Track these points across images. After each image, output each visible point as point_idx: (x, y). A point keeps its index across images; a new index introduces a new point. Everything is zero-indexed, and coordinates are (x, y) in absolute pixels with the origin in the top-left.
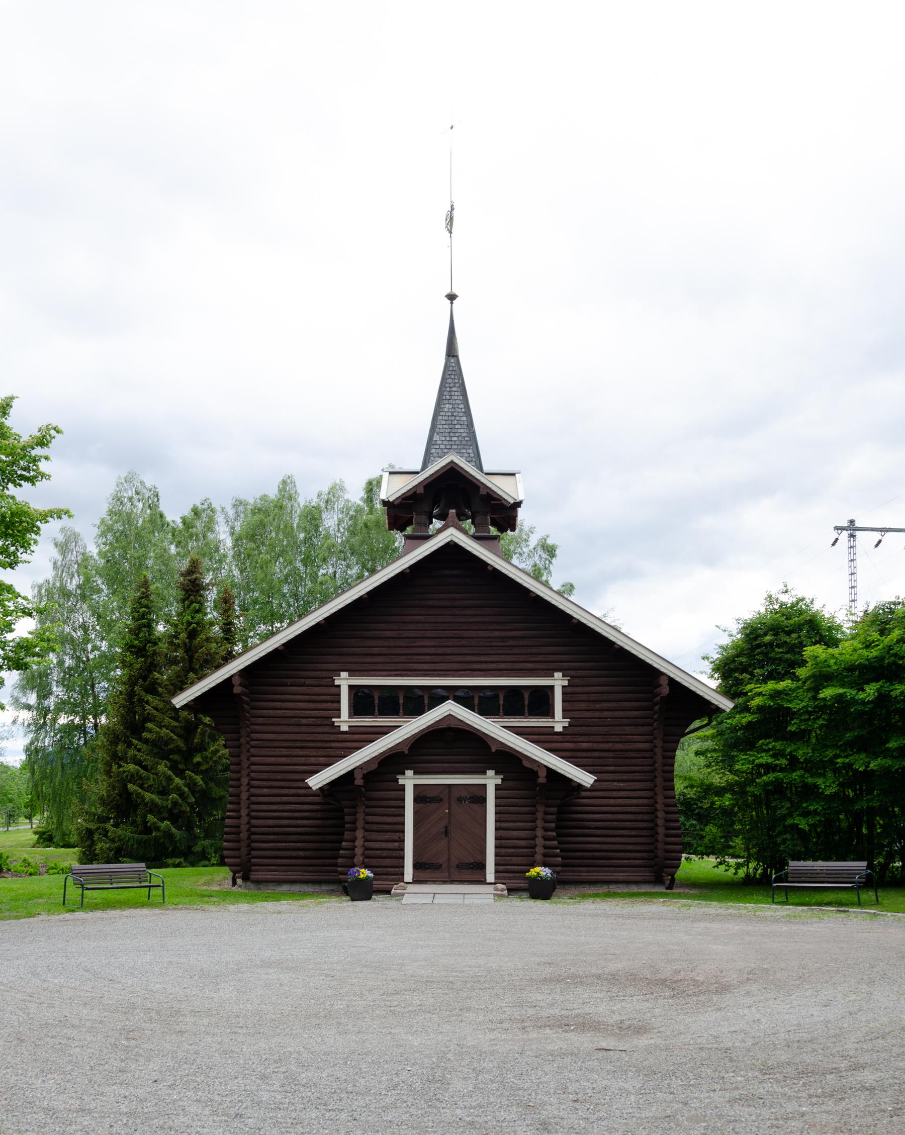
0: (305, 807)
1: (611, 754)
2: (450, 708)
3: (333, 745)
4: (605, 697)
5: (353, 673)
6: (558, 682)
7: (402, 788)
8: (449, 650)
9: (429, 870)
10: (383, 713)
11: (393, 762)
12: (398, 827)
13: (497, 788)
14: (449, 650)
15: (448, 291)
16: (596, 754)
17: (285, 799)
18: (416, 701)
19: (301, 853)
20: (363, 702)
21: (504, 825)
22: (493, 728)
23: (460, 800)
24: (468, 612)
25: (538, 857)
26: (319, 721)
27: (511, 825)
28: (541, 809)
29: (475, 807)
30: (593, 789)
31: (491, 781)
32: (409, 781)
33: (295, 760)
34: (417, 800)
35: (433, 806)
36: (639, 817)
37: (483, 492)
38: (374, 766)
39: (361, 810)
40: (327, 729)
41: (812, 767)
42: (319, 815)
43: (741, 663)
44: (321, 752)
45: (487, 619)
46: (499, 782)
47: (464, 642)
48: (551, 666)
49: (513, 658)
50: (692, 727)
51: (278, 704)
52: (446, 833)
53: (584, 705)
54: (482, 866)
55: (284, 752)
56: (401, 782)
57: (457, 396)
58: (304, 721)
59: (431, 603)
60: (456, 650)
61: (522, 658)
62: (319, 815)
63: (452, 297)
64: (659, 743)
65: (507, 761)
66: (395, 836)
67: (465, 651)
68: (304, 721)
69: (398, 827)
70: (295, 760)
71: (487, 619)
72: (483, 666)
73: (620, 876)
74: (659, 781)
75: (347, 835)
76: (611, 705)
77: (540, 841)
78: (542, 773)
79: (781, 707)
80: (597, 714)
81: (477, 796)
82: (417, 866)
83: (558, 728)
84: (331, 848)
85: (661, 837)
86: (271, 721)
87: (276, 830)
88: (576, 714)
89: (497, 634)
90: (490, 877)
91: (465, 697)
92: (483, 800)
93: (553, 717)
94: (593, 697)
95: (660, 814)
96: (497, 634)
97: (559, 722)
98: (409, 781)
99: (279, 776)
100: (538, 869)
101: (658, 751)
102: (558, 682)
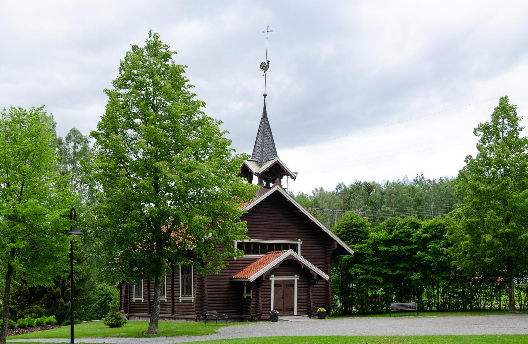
0: (223, 290)
2: (289, 252)
4: (312, 248)
6: (299, 242)
8: (267, 230)
9: (301, 313)
10: (255, 253)
11: (274, 271)
12: (269, 296)
13: (298, 281)
14: (267, 230)
15: (264, 93)
17: (216, 286)
19: (222, 308)
23: (287, 285)
24: (273, 215)
29: (291, 288)
31: (296, 278)
32: (273, 278)
34: (275, 285)
35: (279, 288)
36: (322, 291)
39: (260, 290)
41: (375, 274)
45: (278, 218)
47: (272, 227)
48: (297, 236)
49: (286, 233)
52: (283, 298)
54: (293, 309)
56: (270, 279)
59: (262, 211)
61: (289, 233)
63: (265, 96)
67: (272, 230)
69: (269, 296)
71: (278, 218)
72: (278, 236)
78: (316, 276)
79: (362, 252)
80: (310, 254)
81: (291, 284)
84: (241, 303)
87: (213, 299)
89: (281, 224)
90: (296, 313)
92: (293, 285)
94: (309, 248)
96: (281, 224)
98: (273, 278)
101: (329, 268)
102: (299, 242)
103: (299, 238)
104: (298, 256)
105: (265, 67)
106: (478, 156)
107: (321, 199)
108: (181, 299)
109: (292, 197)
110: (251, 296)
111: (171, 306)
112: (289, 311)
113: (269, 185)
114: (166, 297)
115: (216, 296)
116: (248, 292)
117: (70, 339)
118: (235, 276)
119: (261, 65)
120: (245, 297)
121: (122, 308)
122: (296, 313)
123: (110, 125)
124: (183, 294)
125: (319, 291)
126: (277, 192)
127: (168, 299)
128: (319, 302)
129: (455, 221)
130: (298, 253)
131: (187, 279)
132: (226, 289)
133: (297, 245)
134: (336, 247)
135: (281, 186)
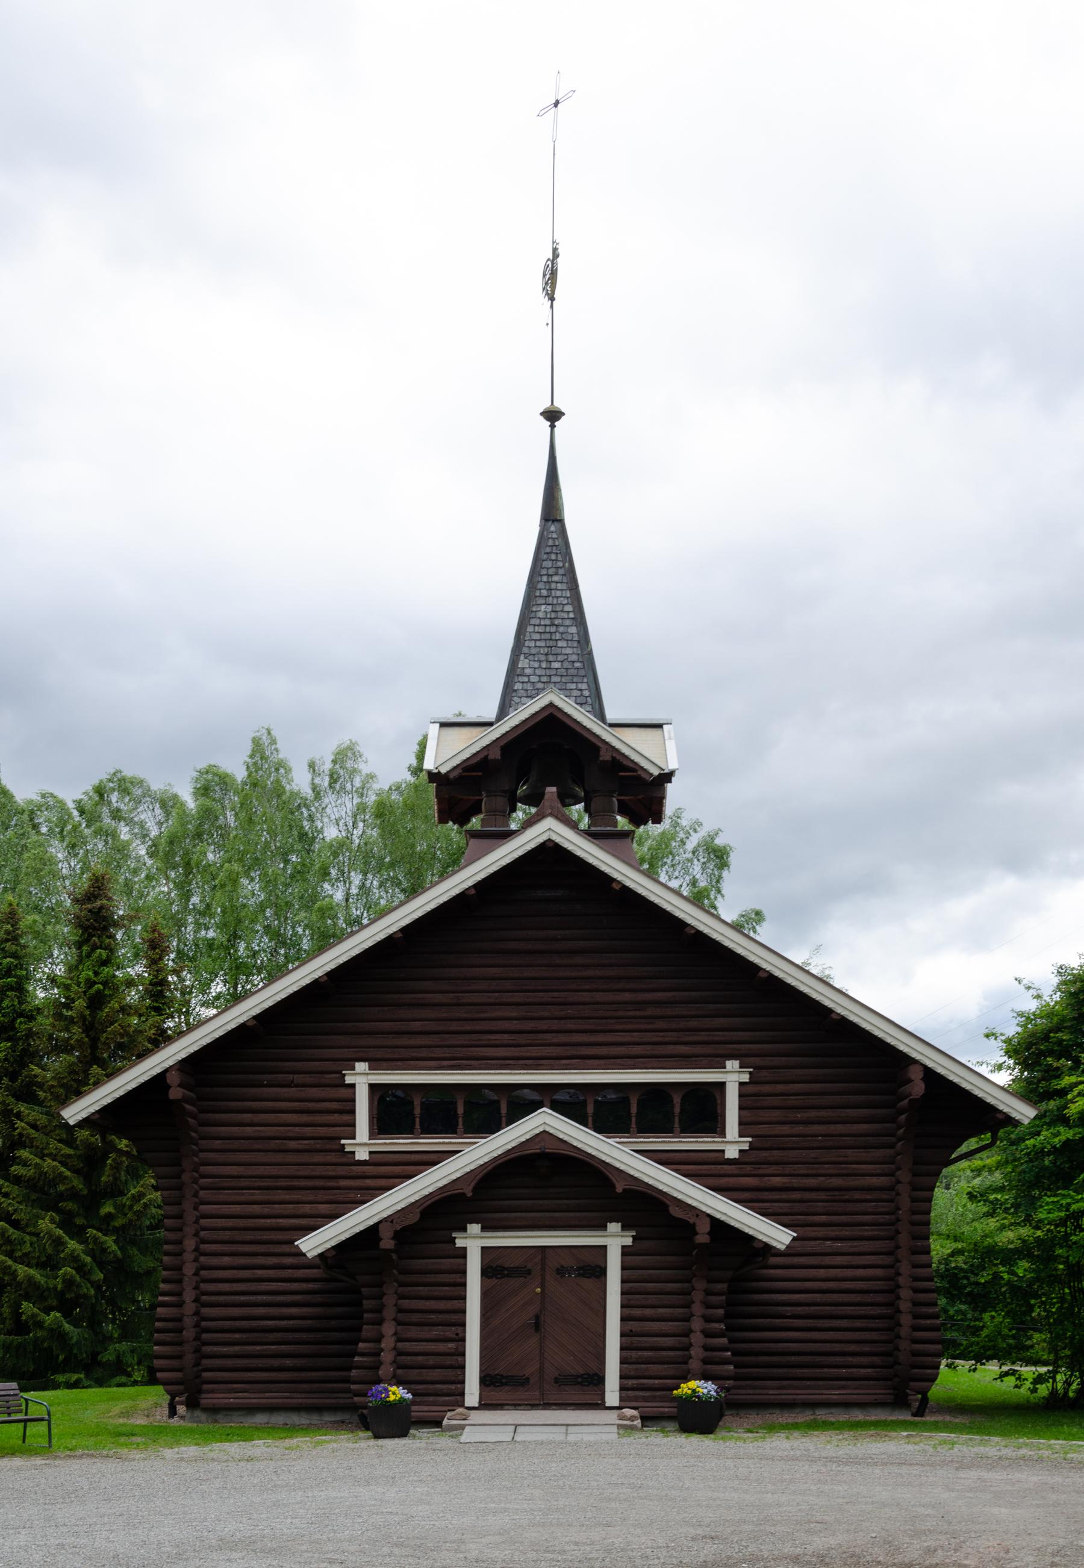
0: (295, 1286)
1: (823, 1195)
3: (343, 1183)
5: (376, 1063)
6: (732, 1076)
7: (463, 1253)
9: (505, 1387)
10: (429, 1130)
11: (446, 1211)
12: (454, 1318)
13: (625, 1251)
16: (796, 1195)
18: (487, 1111)
19: (288, 1362)
20: (393, 1111)
21: (637, 1312)
22: (617, 1152)
23: (561, 1271)
25: (695, 1365)
26: (319, 1144)
27: (648, 1312)
28: (700, 1285)
29: (588, 1283)
30: (790, 1252)
31: (614, 1240)
32: (473, 1242)
33: (277, 1209)
34: (487, 1272)
36: (869, 1298)
37: (605, 756)
38: (414, 1218)
40: (332, 1158)
42: (318, 1298)
43: (1060, 1042)
44: (321, 1196)
46: (629, 1241)
47: (570, 1011)
48: (721, 1049)
50: (964, 1148)
51: (247, 1117)
52: (537, 1326)
53: (776, 1115)
54: (598, 1380)
55: (258, 1195)
56: (459, 1243)
57: (561, 590)
58: (293, 1144)
60: (555, 1025)
62: (318, 1298)
63: (553, 416)
64: (904, 1176)
65: (642, 1207)
66: (450, 1332)
68: (293, 1144)
70: (277, 1209)
73: (834, 1395)
74: (903, 1239)
75: (367, 1331)
76: (824, 1113)
77: (697, 1338)
78: (703, 1228)
80: (800, 1129)
81: (592, 1265)
82: (487, 1380)
83: (732, 1153)
84: (345, 1353)
85: (904, 1331)
86: (236, 1144)
88: (763, 1129)
89: (627, 996)
90: (612, 1397)
91: (572, 1103)
93: (723, 1134)
95: (905, 1293)
96: (627, 996)
97: (732, 1142)
98: (473, 1242)
99: (249, 1236)
100: (693, 1384)
102: (732, 1076)
106: (244, 783)
115: (261, 1311)
122: (612, 1397)
125: (857, 1298)
128: (853, 1348)
131: (914, 1253)
132: (311, 1286)
133: (721, 1086)
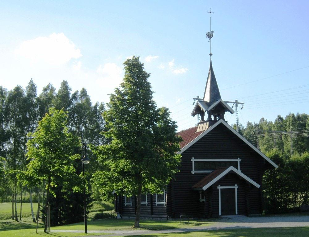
2: (231, 168)
6: (239, 160)
11: (220, 182)
13: (238, 189)
31: (236, 187)
32: (220, 188)
63: (211, 55)
90: (237, 213)
98: (220, 188)
102: (239, 160)
103: (239, 157)
104: (238, 172)
105: (210, 36)
107: (258, 130)
108: (157, 203)
109: (240, 132)
110: (205, 201)
111: (150, 209)
112: (232, 212)
113: (216, 119)
114: (147, 202)
116: (203, 198)
117: (85, 231)
118: (194, 186)
119: (207, 34)
120: (201, 202)
121: (118, 210)
122: (237, 213)
123: (160, 110)
124: (158, 200)
126: (221, 124)
127: (148, 204)
129: (203, 219)
130: (237, 169)
134: (265, 163)
135: (224, 120)
